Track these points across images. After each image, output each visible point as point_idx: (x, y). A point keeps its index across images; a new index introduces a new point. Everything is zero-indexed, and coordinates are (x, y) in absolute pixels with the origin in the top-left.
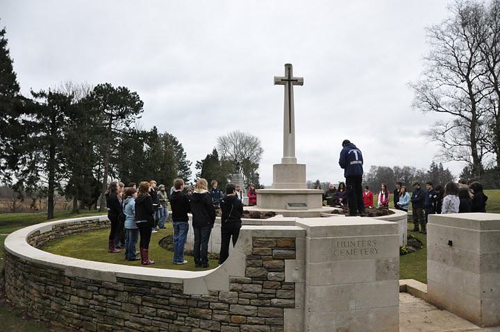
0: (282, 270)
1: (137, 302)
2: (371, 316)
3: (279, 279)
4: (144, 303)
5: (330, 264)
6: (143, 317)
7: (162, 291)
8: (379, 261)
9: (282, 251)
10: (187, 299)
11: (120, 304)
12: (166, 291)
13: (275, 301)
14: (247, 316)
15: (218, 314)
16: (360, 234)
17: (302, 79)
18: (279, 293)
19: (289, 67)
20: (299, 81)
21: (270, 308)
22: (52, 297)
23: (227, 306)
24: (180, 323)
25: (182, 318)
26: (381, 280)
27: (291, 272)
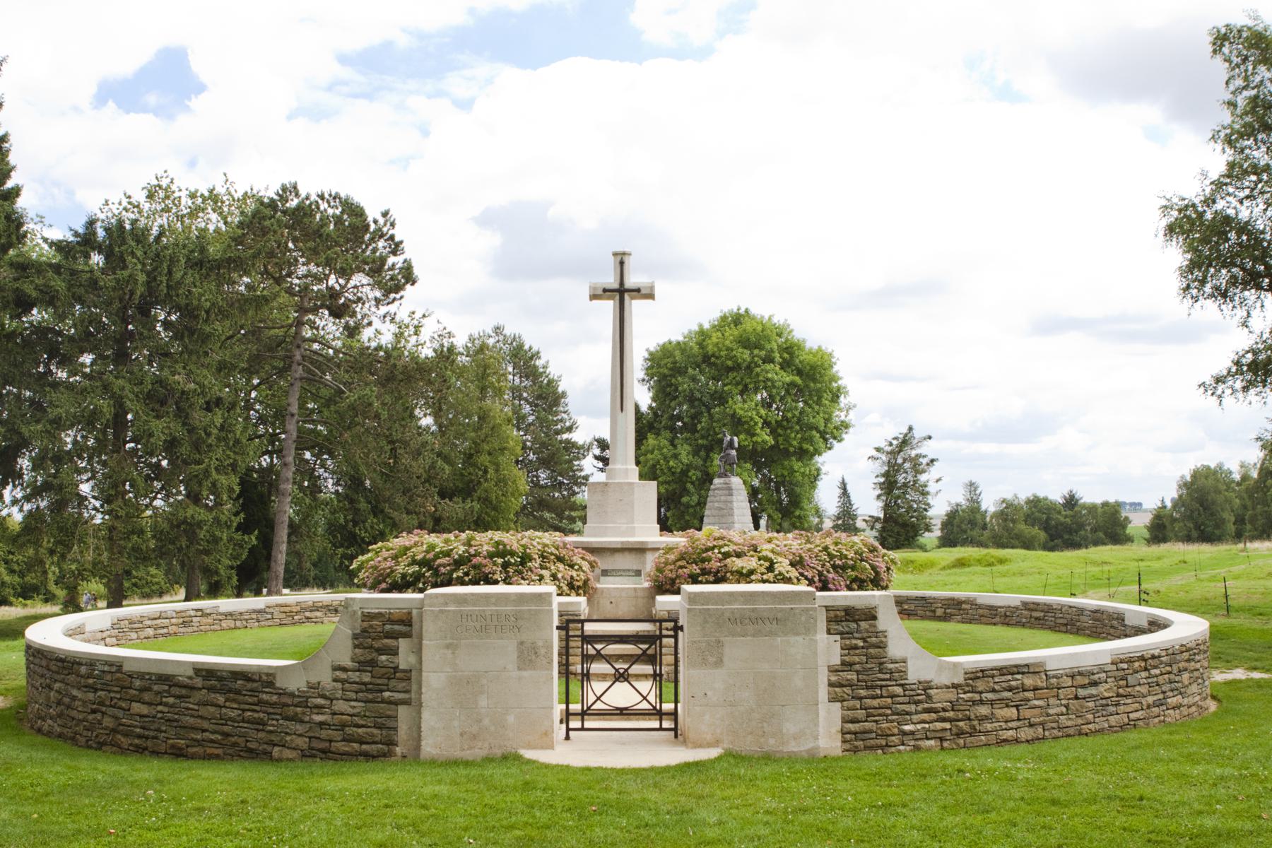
0: (394, 652)
1: (219, 702)
2: (511, 719)
3: (391, 665)
4: (227, 704)
5: (451, 644)
6: (226, 725)
7: (250, 685)
9: (396, 627)
10: (280, 694)
11: (196, 707)
12: (255, 685)
13: (387, 694)
14: (351, 716)
15: (318, 714)
16: (495, 605)
17: (652, 288)
18: (393, 683)
19: (621, 261)
20: (643, 292)
21: (382, 705)
22: (104, 709)
23: (328, 702)
24: (271, 728)
25: (274, 722)
26: (525, 670)
27: (405, 659)
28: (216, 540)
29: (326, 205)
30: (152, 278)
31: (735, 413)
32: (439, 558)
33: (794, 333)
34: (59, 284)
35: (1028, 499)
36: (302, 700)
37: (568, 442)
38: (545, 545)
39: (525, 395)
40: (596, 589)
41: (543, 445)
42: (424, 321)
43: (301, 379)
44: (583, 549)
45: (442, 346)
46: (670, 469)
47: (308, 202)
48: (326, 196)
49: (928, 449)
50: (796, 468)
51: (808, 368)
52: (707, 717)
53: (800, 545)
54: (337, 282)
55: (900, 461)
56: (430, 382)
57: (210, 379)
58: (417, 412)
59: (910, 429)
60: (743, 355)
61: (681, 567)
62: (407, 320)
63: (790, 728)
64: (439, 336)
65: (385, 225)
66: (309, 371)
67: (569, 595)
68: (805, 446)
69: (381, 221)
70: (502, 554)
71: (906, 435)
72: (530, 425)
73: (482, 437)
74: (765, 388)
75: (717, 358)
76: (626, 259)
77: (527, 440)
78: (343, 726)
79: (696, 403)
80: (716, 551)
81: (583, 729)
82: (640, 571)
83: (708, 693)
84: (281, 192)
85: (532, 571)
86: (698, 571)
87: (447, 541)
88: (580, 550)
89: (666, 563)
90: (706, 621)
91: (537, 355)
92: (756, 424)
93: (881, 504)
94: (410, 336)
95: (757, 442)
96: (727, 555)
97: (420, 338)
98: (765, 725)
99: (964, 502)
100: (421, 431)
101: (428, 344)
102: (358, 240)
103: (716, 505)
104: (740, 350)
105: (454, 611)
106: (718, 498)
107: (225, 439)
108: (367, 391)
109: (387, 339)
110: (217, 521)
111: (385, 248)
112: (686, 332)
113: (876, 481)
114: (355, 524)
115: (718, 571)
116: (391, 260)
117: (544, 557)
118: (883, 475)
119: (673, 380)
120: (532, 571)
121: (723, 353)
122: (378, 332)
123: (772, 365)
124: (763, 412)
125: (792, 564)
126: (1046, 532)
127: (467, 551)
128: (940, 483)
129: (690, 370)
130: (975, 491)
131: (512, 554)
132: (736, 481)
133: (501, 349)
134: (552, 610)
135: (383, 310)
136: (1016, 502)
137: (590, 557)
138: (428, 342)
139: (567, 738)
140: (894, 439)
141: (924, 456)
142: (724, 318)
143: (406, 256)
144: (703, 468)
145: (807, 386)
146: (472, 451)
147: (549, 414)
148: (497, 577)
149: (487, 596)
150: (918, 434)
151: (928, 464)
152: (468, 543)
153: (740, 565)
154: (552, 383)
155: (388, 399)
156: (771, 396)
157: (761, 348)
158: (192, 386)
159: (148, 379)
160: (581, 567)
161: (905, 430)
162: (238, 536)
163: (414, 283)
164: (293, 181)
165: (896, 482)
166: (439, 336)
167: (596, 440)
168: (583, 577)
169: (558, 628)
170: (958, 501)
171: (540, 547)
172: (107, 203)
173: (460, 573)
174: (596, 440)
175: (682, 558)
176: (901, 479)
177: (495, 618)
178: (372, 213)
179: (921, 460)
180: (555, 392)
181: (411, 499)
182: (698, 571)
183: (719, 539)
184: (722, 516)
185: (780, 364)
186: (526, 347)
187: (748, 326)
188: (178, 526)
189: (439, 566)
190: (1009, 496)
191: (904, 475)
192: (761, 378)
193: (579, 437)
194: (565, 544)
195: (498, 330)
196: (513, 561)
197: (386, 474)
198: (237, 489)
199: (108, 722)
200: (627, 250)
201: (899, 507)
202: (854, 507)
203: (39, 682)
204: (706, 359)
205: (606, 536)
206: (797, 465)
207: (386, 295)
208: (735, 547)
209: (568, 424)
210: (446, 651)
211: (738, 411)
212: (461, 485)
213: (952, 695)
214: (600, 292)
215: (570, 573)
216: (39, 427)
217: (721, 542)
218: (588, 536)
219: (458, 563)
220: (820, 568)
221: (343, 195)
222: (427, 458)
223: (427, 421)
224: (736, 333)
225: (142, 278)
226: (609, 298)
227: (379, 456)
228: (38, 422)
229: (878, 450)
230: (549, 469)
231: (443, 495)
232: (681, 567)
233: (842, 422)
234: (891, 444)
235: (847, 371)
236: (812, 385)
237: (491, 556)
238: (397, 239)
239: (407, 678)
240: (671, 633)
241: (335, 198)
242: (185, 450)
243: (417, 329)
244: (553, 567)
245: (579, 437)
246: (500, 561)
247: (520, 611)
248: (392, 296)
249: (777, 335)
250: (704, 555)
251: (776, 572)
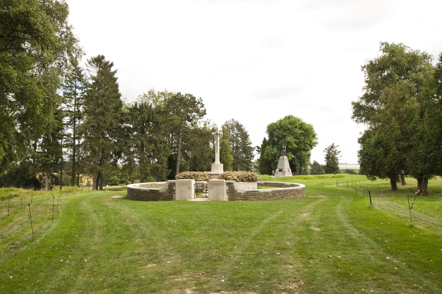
0: (173, 187)
28: (162, 171)
30: (149, 116)
34: (130, 117)
36: (162, 194)
37: (250, 147)
45: (214, 127)
46: (272, 154)
49: (338, 149)
50: (303, 152)
55: (331, 152)
57: (161, 137)
59: (333, 144)
60: (290, 126)
62: (206, 121)
63: (221, 197)
68: (305, 148)
69: (199, 100)
78: (167, 197)
107: (164, 150)
108: (195, 139)
110: (163, 167)
114: (196, 167)
116: (201, 109)
121: (285, 126)
125: (237, 177)
129: (277, 130)
142: (286, 117)
149: (186, 181)
150: (335, 145)
152: (190, 174)
154: (246, 133)
158: (157, 139)
159: (148, 137)
161: (332, 144)
162: (167, 170)
163: (206, 114)
172: (140, 95)
186: (239, 124)
187: (291, 119)
188: (155, 168)
195: (233, 120)
198: (167, 160)
199: (138, 197)
203: (129, 192)
204: (281, 127)
206: (303, 152)
207: (200, 117)
209: (250, 142)
213: (244, 194)
216: (126, 148)
219: (189, 176)
221: (191, 94)
224: (288, 121)
225: (147, 116)
228: (126, 146)
229: (326, 149)
235: (317, 130)
237: (193, 175)
238: (203, 104)
239: (174, 191)
242: (156, 152)
243: (209, 123)
245: (252, 146)
248: (201, 117)
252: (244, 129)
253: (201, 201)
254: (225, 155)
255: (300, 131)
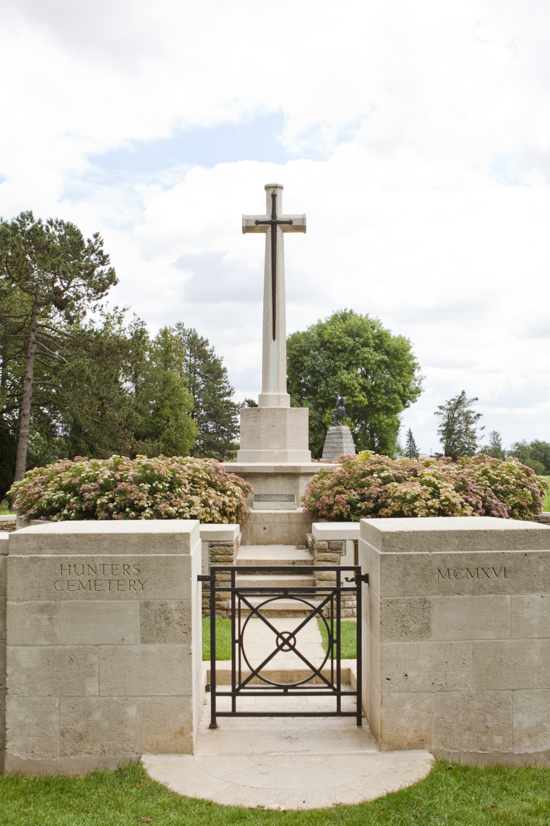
2: (132, 711)
5: (47, 606)
8: (147, 605)
17: (303, 220)
20: (295, 223)
26: (152, 642)
29: (54, 229)
31: (342, 381)
32: (85, 483)
33: (382, 326)
35: (533, 443)
37: (228, 402)
38: (196, 470)
39: (198, 370)
40: (250, 514)
41: (211, 405)
42: (125, 313)
43: (35, 354)
44: (236, 474)
47: (39, 226)
48: (54, 222)
49: (475, 408)
51: (393, 350)
52: (408, 707)
53: (458, 469)
54: (62, 284)
55: (456, 415)
56: (127, 356)
58: (121, 379)
59: (463, 393)
61: (339, 493)
62: (112, 313)
64: (135, 324)
65: (96, 244)
66: (42, 348)
67: (220, 522)
68: (389, 404)
69: (93, 240)
70: (149, 479)
71: (460, 397)
72: (202, 391)
73: (166, 396)
74: (363, 365)
75: (330, 343)
76: (278, 191)
77: (200, 401)
79: (317, 374)
80: (375, 475)
81: (234, 713)
82: (293, 496)
83: (410, 674)
84: (20, 219)
85: (180, 496)
86: (358, 497)
87: (95, 467)
88: (233, 475)
89: (323, 488)
90: (406, 574)
91: (206, 343)
92: (356, 388)
93: (443, 445)
94: (114, 324)
95: (356, 401)
96: (386, 480)
97: (122, 326)
98: (489, 717)
99: (490, 445)
100: (121, 392)
101: (127, 330)
102: (77, 255)
103: (331, 445)
104: (347, 338)
105: (50, 559)
106: (332, 440)
108: (81, 361)
109: (99, 326)
111: (96, 260)
112: (310, 325)
113: (439, 429)
115: (378, 497)
117: (194, 482)
118: (445, 425)
119: (300, 359)
120: (180, 496)
121: (335, 340)
122: (92, 321)
123: (368, 348)
124: (361, 381)
126: (545, 465)
127: (113, 476)
128: (484, 430)
130: (497, 437)
131: (161, 479)
132: (345, 429)
133: (182, 338)
134: (188, 560)
135: (93, 303)
136: (525, 445)
137: (243, 482)
138: (127, 329)
139: (213, 726)
140: (452, 400)
141: (473, 412)
142: (335, 317)
143: (111, 265)
144: (319, 419)
145: (393, 363)
146: (159, 406)
147: (215, 383)
148: (143, 503)
151: (475, 418)
152: (115, 468)
153: (404, 490)
154: (216, 362)
155: (96, 367)
156: (367, 370)
157: (359, 335)
160: (233, 493)
161: (460, 394)
164: (29, 211)
165: (453, 430)
166: (135, 324)
167: (247, 401)
168: (235, 502)
169: (200, 578)
170: (486, 444)
171: (190, 472)
173: (104, 500)
174: (247, 401)
175: (339, 483)
176: (457, 427)
177: (108, 568)
178: (87, 235)
179: (471, 415)
180: (219, 368)
181: (115, 440)
182: (358, 497)
183: (375, 463)
184: (336, 453)
185: (374, 347)
186: (199, 338)
187: (351, 322)
189: (84, 491)
190: (520, 441)
191: (459, 425)
192: (360, 357)
193: (237, 399)
194: (217, 470)
195: (180, 326)
196: (161, 487)
197: (98, 423)
200: (279, 182)
201: (456, 447)
202: (417, 449)
204: (323, 344)
205: (259, 461)
206: (383, 417)
208: (395, 472)
209: (227, 390)
210: (39, 616)
211: (343, 379)
212: (151, 431)
214: (253, 224)
215: (222, 499)
217: (379, 467)
218: (240, 462)
219: (105, 488)
220: (483, 494)
222: (126, 410)
223: (128, 386)
224: (344, 326)
226: (261, 231)
227: (89, 409)
229: (441, 408)
230: (215, 421)
231: (137, 437)
232: (339, 493)
233: (417, 388)
234: (449, 404)
236: (396, 362)
237: (137, 481)
238: (105, 254)
240: (353, 585)
241: (60, 224)
244: (203, 493)
246: (147, 486)
247: (144, 559)
249: (372, 327)
250: (363, 480)
251: (443, 498)
252: (212, 351)
253: (191, 676)
254: (174, 418)
255: (379, 357)
